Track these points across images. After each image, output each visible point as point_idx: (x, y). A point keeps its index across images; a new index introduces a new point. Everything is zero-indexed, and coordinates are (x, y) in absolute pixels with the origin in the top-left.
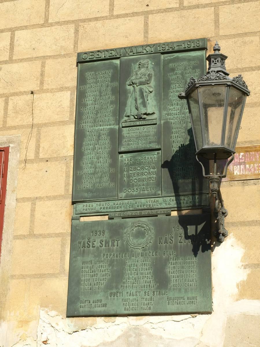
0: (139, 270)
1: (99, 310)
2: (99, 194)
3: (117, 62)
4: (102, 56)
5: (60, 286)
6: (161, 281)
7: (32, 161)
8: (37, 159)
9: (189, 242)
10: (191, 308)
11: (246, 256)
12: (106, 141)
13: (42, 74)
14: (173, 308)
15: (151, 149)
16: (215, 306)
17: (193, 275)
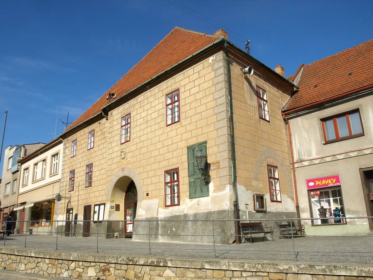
0: (199, 189)
1: (194, 197)
2: (192, 175)
3: (193, 148)
4: (190, 147)
5: (188, 193)
6: (202, 191)
7: (182, 170)
8: (183, 169)
9: (205, 183)
10: (206, 196)
11: (214, 185)
12: (192, 164)
13: (182, 151)
14: (204, 196)
15: (249, 223)
16: (210, 195)
17: (206, 189)
